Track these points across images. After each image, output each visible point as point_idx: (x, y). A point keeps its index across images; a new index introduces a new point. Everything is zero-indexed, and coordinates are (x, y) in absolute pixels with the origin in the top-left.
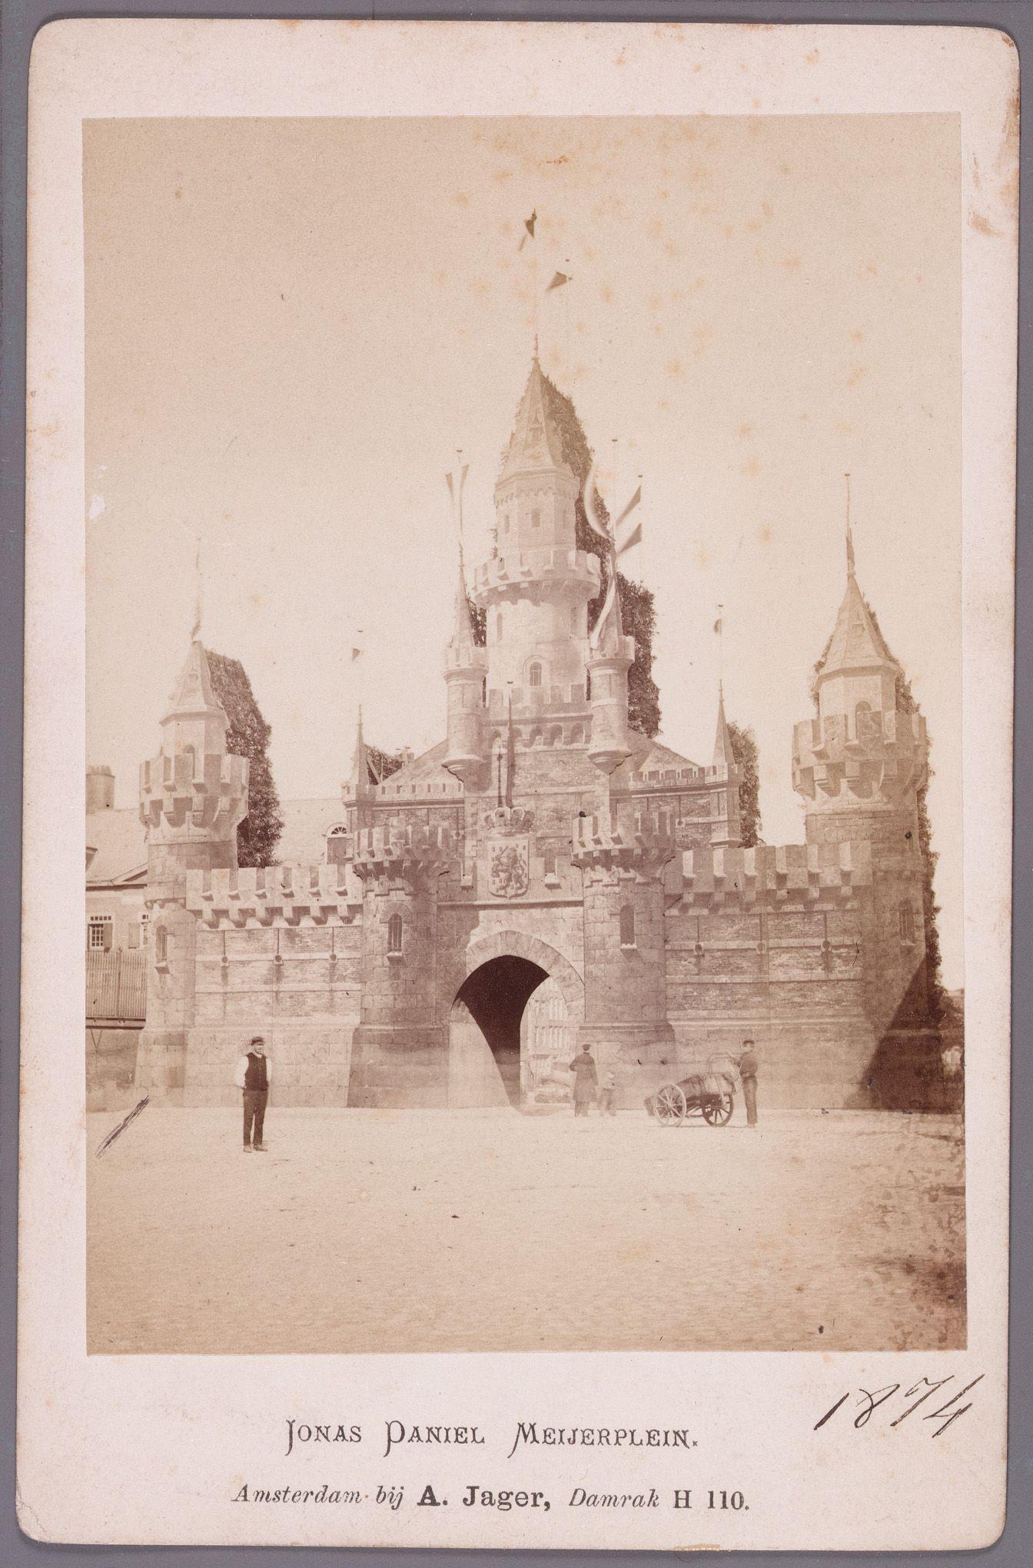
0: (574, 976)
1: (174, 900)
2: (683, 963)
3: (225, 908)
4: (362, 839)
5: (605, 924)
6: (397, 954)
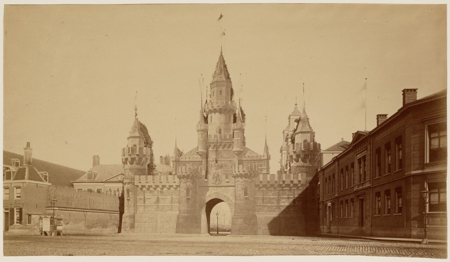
0: (232, 203)
1: (131, 183)
2: (259, 201)
3: (144, 185)
4: (180, 169)
5: (240, 191)
6: (188, 197)
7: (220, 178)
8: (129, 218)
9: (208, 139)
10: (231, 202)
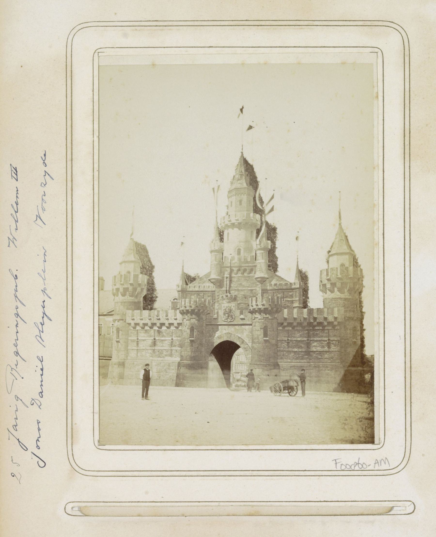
1: (122, 320)
2: (283, 344)
5: (258, 331)
7: (233, 313)
8: (118, 366)
9: (224, 262)
10: (247, 346)
